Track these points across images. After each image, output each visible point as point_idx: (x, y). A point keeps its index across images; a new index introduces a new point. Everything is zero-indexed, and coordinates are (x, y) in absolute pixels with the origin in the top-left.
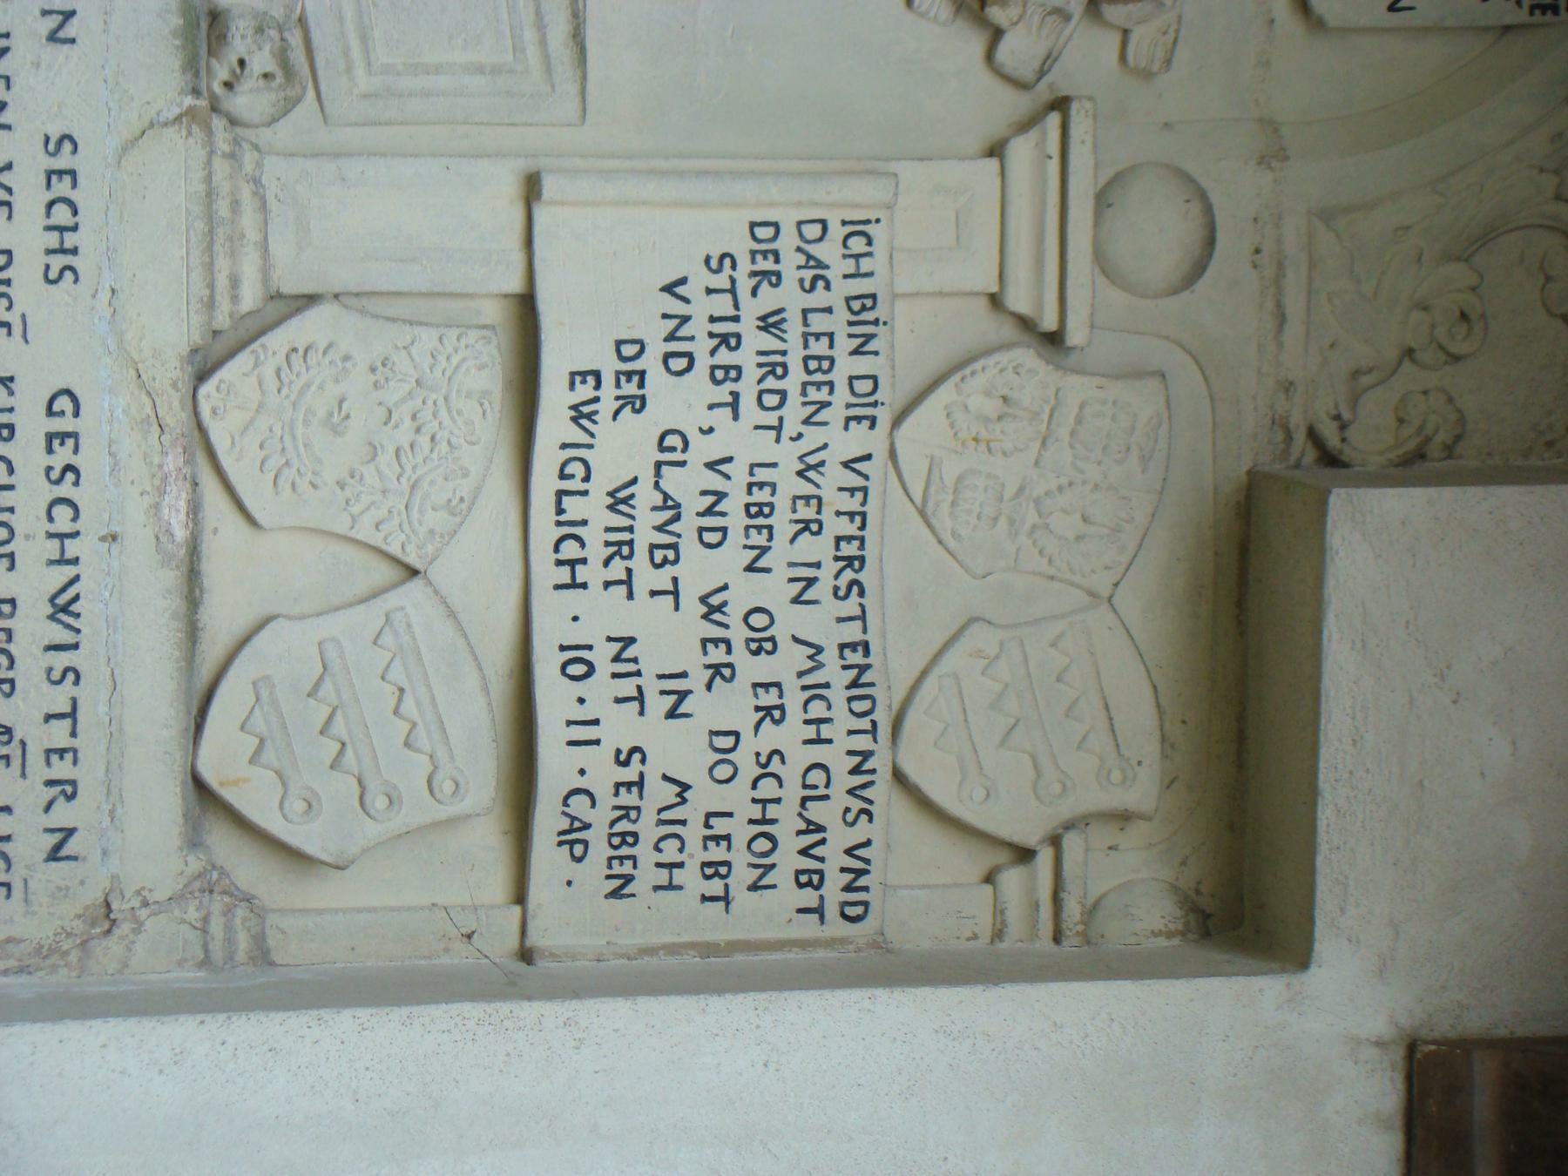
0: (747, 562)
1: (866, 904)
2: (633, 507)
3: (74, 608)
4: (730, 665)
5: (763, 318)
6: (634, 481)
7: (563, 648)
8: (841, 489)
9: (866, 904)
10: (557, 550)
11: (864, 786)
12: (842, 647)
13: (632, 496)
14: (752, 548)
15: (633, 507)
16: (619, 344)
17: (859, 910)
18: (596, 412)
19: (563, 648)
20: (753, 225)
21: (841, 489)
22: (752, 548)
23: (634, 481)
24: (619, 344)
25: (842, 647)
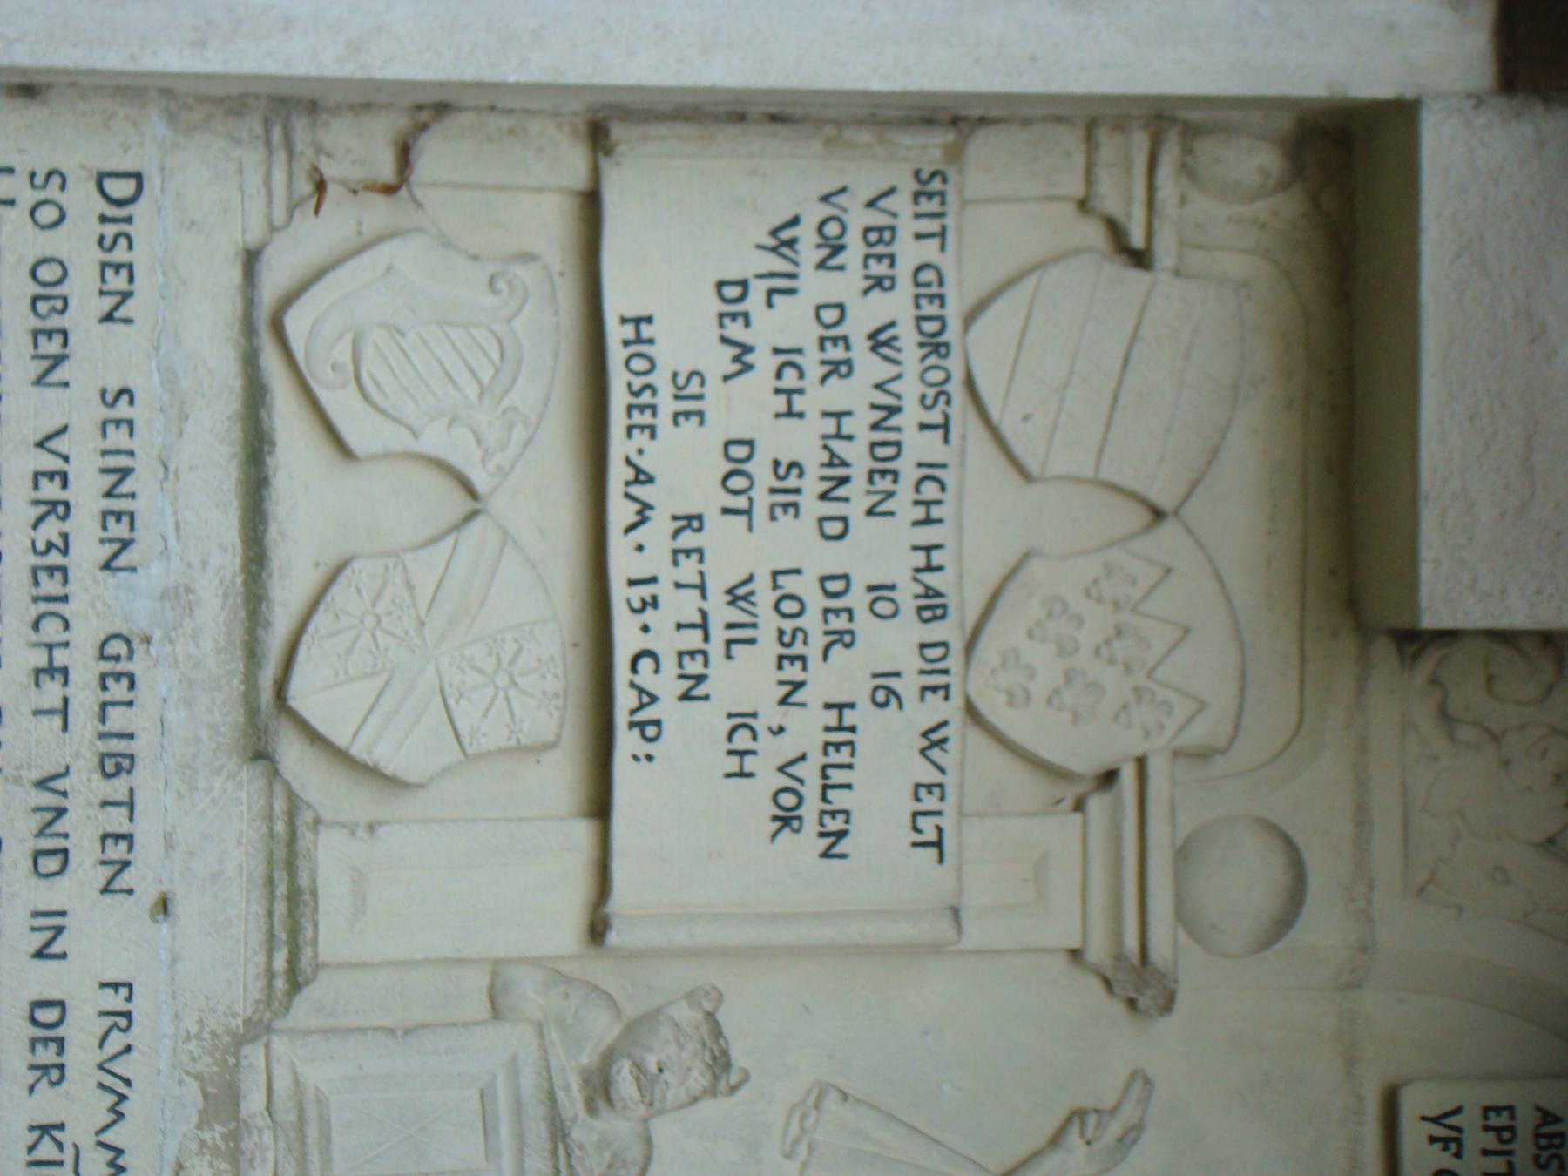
0: (106, 487)
1: (898, 444)
2: (753, 604)
3: (752, 599)
4: (851, 632)
5: (730, 591)
6: (750, 579)
7: (730, 716)
8: (103, 985)
9: (898, 444)
10: (730, 737)
11: (642, 706)
12: (681, 654)
13: (752, 593)
14: (111, 541)
15: (753, 604)
16: (721, 285)
17: (890, 451)
18: (752, 593)
19: (730, 716)
20: (923, 646)
21: (103, 985)
22: (111, 541)
23: (750, 579)
24: (721, 285)
25: (681, 654)
